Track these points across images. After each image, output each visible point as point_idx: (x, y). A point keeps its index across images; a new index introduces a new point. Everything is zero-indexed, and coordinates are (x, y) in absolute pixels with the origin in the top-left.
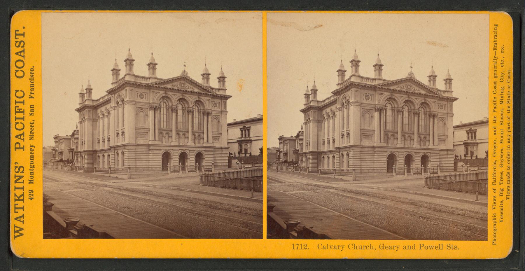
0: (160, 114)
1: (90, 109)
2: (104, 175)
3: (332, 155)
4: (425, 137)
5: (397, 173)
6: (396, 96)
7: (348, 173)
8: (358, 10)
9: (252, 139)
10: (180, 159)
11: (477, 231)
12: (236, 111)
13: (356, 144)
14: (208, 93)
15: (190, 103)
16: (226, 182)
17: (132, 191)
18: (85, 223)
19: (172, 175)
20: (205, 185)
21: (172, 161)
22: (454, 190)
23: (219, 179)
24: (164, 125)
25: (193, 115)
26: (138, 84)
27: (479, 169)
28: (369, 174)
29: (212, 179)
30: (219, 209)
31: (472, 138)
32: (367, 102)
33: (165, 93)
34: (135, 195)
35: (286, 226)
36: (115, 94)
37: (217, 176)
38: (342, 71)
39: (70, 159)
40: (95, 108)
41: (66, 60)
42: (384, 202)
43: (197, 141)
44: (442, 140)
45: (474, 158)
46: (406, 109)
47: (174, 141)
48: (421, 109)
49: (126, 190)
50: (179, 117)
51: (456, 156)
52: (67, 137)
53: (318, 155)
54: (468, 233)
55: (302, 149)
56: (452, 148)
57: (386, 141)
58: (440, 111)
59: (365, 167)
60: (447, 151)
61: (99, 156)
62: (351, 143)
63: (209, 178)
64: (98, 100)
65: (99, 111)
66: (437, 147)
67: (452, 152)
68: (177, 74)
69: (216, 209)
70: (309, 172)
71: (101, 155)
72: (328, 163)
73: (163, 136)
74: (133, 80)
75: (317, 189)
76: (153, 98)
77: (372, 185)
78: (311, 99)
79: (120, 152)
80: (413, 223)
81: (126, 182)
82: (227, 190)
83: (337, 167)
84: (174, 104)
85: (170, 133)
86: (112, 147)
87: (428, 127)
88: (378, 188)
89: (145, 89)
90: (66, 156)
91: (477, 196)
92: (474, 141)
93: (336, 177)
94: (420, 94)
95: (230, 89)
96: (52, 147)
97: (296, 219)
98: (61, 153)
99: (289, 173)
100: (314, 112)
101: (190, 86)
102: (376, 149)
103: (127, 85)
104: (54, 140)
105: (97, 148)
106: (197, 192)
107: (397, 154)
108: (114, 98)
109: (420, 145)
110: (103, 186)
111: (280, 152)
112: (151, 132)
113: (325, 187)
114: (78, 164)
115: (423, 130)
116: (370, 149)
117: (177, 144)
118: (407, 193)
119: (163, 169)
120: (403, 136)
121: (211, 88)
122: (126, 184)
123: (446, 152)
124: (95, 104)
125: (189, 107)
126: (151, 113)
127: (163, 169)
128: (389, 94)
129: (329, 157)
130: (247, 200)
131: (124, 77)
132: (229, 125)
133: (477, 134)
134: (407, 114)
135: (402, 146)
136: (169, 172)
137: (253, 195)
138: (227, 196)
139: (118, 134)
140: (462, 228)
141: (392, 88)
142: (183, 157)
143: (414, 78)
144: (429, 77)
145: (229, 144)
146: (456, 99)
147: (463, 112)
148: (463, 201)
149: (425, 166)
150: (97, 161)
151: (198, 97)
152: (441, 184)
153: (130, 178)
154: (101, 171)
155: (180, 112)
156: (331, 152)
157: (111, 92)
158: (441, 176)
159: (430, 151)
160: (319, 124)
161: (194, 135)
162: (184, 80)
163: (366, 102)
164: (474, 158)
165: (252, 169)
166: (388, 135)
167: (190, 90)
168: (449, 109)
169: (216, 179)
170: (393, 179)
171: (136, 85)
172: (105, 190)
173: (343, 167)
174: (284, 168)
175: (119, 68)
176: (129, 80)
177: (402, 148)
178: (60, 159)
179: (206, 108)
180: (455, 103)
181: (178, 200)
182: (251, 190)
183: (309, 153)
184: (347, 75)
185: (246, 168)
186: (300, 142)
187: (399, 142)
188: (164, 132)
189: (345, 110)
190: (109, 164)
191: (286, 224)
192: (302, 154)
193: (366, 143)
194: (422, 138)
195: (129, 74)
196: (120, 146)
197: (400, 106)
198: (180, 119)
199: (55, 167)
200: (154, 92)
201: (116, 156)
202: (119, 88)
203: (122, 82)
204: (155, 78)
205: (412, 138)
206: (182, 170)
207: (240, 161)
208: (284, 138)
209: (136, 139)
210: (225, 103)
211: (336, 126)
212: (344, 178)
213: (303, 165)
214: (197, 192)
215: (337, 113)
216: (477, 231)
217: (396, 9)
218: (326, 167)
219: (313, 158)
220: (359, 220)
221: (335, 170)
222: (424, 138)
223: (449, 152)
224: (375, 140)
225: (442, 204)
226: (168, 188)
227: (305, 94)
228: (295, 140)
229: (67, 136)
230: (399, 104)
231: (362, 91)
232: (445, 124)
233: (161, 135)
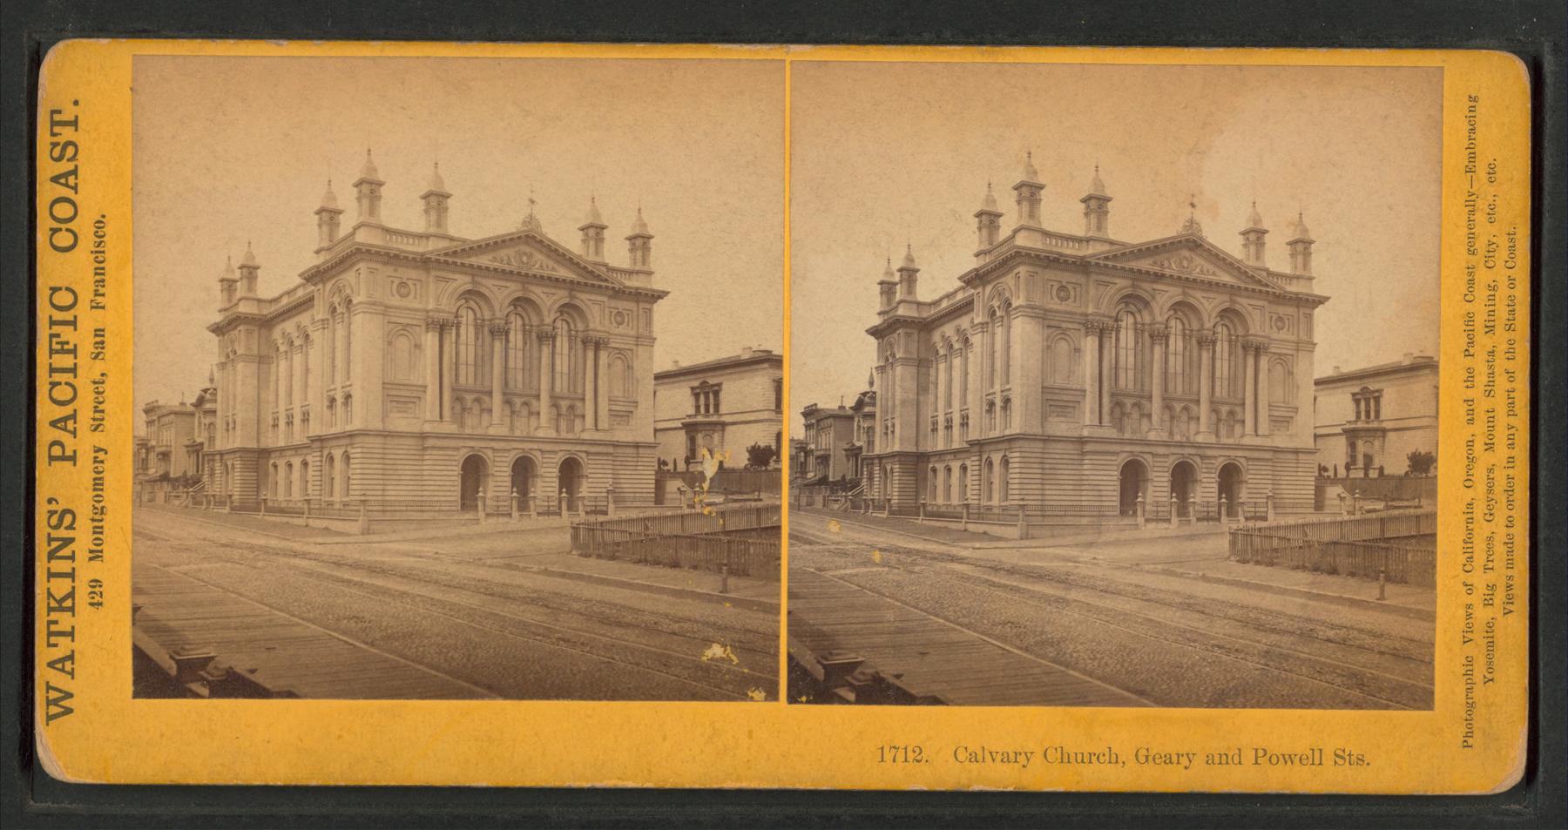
0: (457, 343)
1: (251, 326)
2: (291, 520)
3: (959, 463)
4: (571, 407)
5: (1148, 516)
6: (489, 285)
7: (1006, 516)
9: (1384, 425)
10: (561, 479)
11: (1381, 690)
12: (682, 335)
13: (370, 427)
14: (1258, 288)
15: (1205, 317)
16: (650, 547)
17: (372, 569)
18: (233, 664)
19: (487, 524)
20: (1244, 562)
21: (491, 483)
22: (657, 563)
23: (626, 538)
24: (467, 378)
25: (554, 346)
26: (1052, 256)
27: (1387, 508)
28: (1068, 521)
29: (608, 537)
30: (628, 625)
31: (707, 410)
32: (1062, 307)
33: (473, 282)
34: (379, 582)
35: (175, 666)
36: (324, 282)
37: (623, 527)
38: (989, 214)
39: (190, 474)
40: (266, 323)
41: (194, 186)
42: (1108, 603)
43: (563, 424)
44: (623, 416)
45: (1373, 474)
46: (516, 323)
47: (496, 423)
48: (1219, 329)
49: (356, 566)
50: (511, 353)
51: (663, 463)
52: (184, 409)
53: (917, 463)
54: (1356, 694)
55: (871, 443)
56: (1310, 444)
57: (1119, 424)
58: (1275, 336)
59: (393, 493)
60: (637, 446)
61: (934, 470)
62: (1016, 428)
63: (598, 533)
64: (936, 303)
65: (277, 333)
66: (1268, 442)
67: (649, 451)
69: (619, 624)
70: (232, 509)
71: (940, 467)
72: (948, 488)
73: (1123, 414)
74: (1039, 246)
75: (913, 563)
76: (438, 295)
77: (1074, 552)
78: (898, 297)
79: (996, 458)
80: (1193, 665)
81: (351, 542)
82: (646, 570)
83: (972, 500)
84: (1159, 319)
85: (486, 399)
86: (972, 444)
87: (1240, 382)
88: (437, 557)
89: (416, 268)
90: (180, 469)
91: (725, 580)
92: (1375, 425)
93: (971, 527)
94: (557, 280)
95: (1325, 276)
96: (799, 442)
97: (851, 650)
98: (165, 456)
99: (834, 515)
100: (249, 332)
101: (1207, 266)
102: (1088, 447)
103: (1018, 260)
104: (803, 420)
105: (269, 441)
106: (563, 575)
108: (323, 294)
109: (1217, 435)
110: (285, 555)
111: (807, 453)
112: (431, 394)
113: (277, 552)
114: (215, 487)
115: (565, 385)
116: (1071, 446)
117: (504, 431)
118: (517, 568)
119: (464, 507)
120: (1167, 406)
121: (1270, 274)
122: (1008, 555)
123: (631, 451)
124: (925, 315)
125: (1202, 328)
126: (430, 340)
127: (464, 507)
128: (468, 279)
129: (949, 470)
130: (708, 598)
131: (353, 234)
132: (659, 377)
133: (722, 395)
134: (520, 336)
135: (504, 431)
136: (1140, 520)
137: (1382, 591)
138: (649, 588)
139: (992, 404)
140: (1339, 680)
141: (474, 260)
142: (523, 470)
143: (1201, 238)
144: (1243, 234)
145: (661, 437)
146: (661, 295)
147: (1343, 339)
148: (680, 594)
149: (1231, 498)
150: (270, 479)
151: (561, 297)
152: (1276, 550)
153: (366, 531)
154: (939, 515)
155: (516, 338)
156: (956, 453)
157: (315, 276)
158: (1278, 528)
159: (584, 448)
160: (923, 370)
161: (555, 406)
162: (527, 243)
163: (1055, 307)
164: (1373, 474)
165: (1383, 514)
166: (1120, 406)
167: (546, 273)
168: (642, 321)
169: (618, 537)
170: (478, 529)
172: (295, 568)
173: (990, 498)
174: (160, 496)
175: (340, 205)
176: (1029, 244)
177: (1165, 444)
178: (161, 472)
179: (591, 326)
180: (1319, 311)
181: (507, 597)
182: (720, 571)
183: (893, 455)
184: (346, 224)
185: (1369, 511)
186: (207, 421)
187: (1203, 428)
188: (469, 398)
189: (999, 331)
190: (965, 493)
191: (824, 667)
192: (870, 461)
193: (1059, 427)
194: (1224, 415)
195: (1028, 229)
196: (337, 437)
197: (498, 315)
198: (516, 360)
199: (804, 500)
200: (439, 279)
201: (985, 471)
202: (337, 264)
203: (341, 250)
205: (1193, 415)
206: (1179, 515)
207: (1351, 491)
208: (817, 411)
209: (1044, 419)
210: (1310, 317)
211: (970, 378)
212: (995, 530)
213: (875, 493)
214: (563, 575)
215: (976, 340)
216: (1381, 690)
218: (940, 501)
219: (903, 472)
220: (1038, 656)
221: (967, 506)
222: (1228, 414)
223: (1301, 456)
224: (427, 416)
225: (1279, 608)
226: (478, 561)
227: (881, 283)
228: (851, 418)
229: (182, 404)
230: (497, 307)
232: (1291, 373)
233: (1117, 411)
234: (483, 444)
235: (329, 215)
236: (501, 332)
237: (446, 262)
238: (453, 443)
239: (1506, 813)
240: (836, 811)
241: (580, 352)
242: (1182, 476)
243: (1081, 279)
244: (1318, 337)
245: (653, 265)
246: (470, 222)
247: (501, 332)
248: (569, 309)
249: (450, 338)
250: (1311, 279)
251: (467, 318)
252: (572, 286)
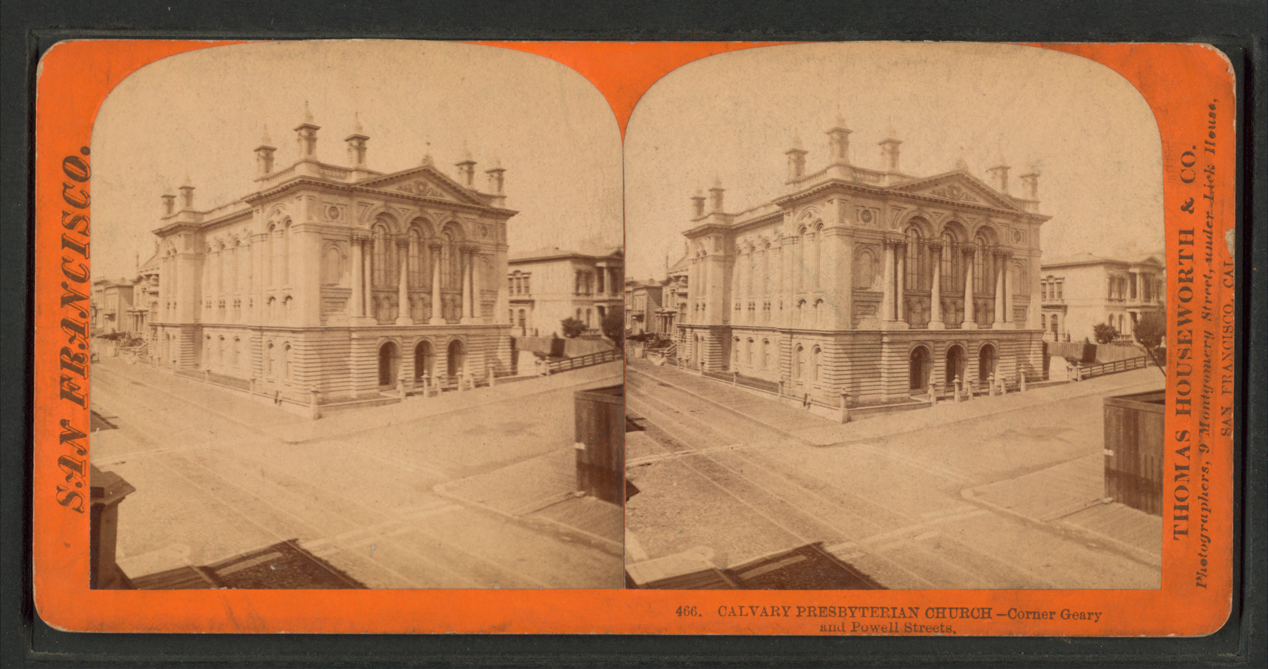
4: (453, 300)
6: (929, 213)
8: (860, 39)
33: (385, 206)
58: (1016, 246)
68: (413, 163)
76: (357, 217)
89: (340, 195)
107: (965, 345)
121: (480, 195)
159: (399, 333)
167: (971, 203)
171: (324, 185)
184: (281, 161)
200: (360, 204)
204: (364, 171)
217: (938, 36)
231: (326, 198)
234: (926, 337)
235: (798, 156)
237: (367, 191)
238: (905, 338)
239: (1222, 660)
240: (682, 658)
241: (991, 262)
242: (422, 352)
244: (509, 242)
245: (506, 190)
246: (387, 158)
247: (936, 249)
248: (451, 226)
251: (380, 232)
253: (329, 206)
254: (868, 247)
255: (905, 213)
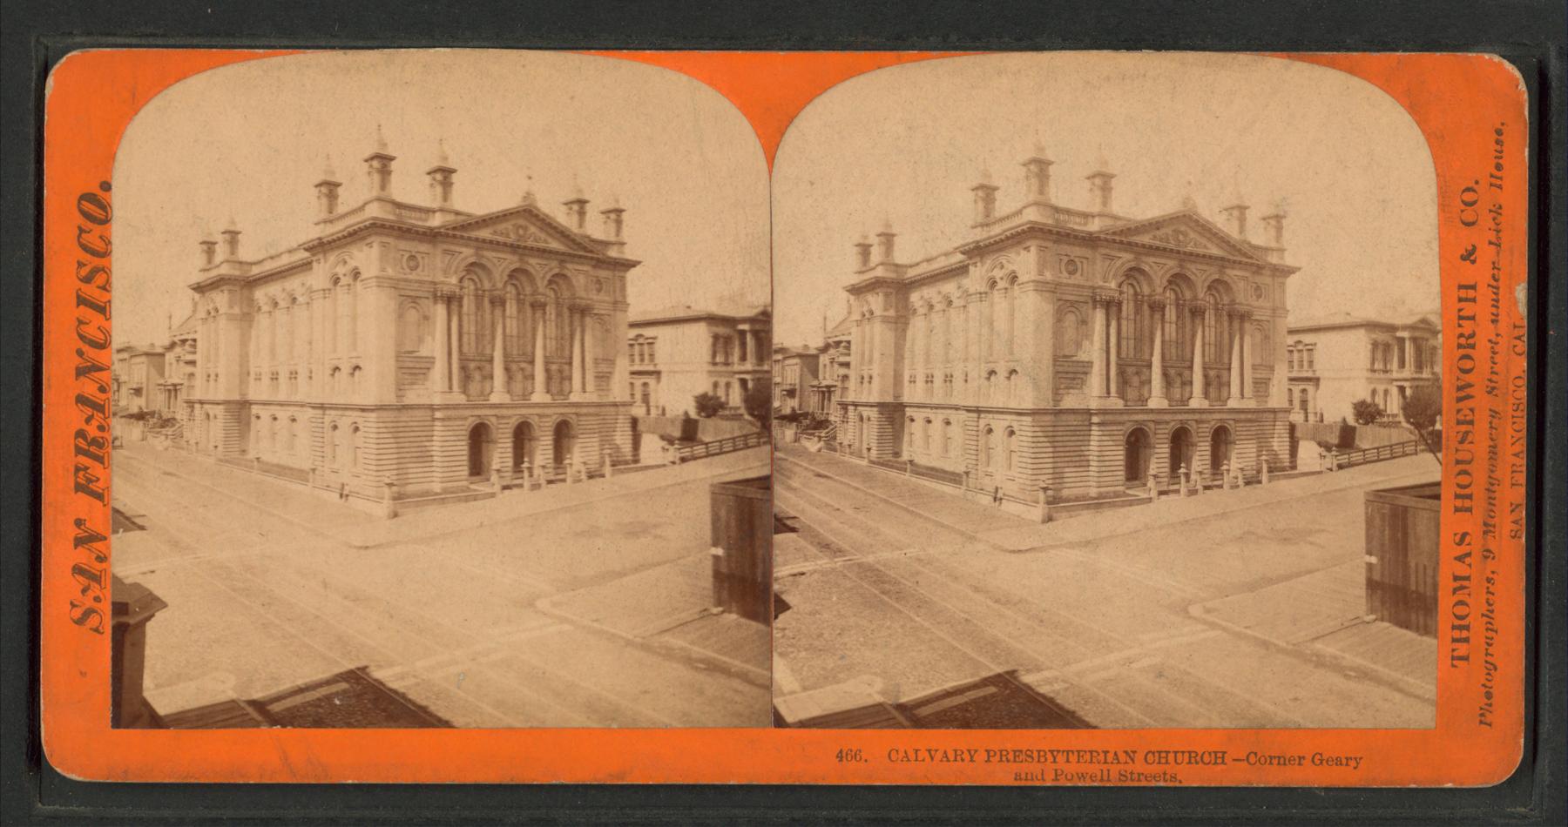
4: (560, 371)
6: (1148, 264)
33: (476, 254)
58: (1256, 304)
68: (511, 202)
76: (441, 269)
89: (421, 241)
107: (1193, 427)
121: (594, 241)
171: (400, 229)
184: (348, 199)
200: (446, 252)
210: (623, 279)
217: (1159, 45)
231: (403, 245)
235: (987, 192)
236: (539, 307)
237: (454, 236)
242: (522, 435)
243: (1087, 252)
244: (630, 300)
245: (626, 235)
246: (478, 195)
247: (1157, 308)
248: (558, 279)
249: (454, 307)
250: (623, 244)
251: (470, 287)
252: (563, 258)
253: (407, 255)
254: (1073, 305)
255: (1119, 263)
